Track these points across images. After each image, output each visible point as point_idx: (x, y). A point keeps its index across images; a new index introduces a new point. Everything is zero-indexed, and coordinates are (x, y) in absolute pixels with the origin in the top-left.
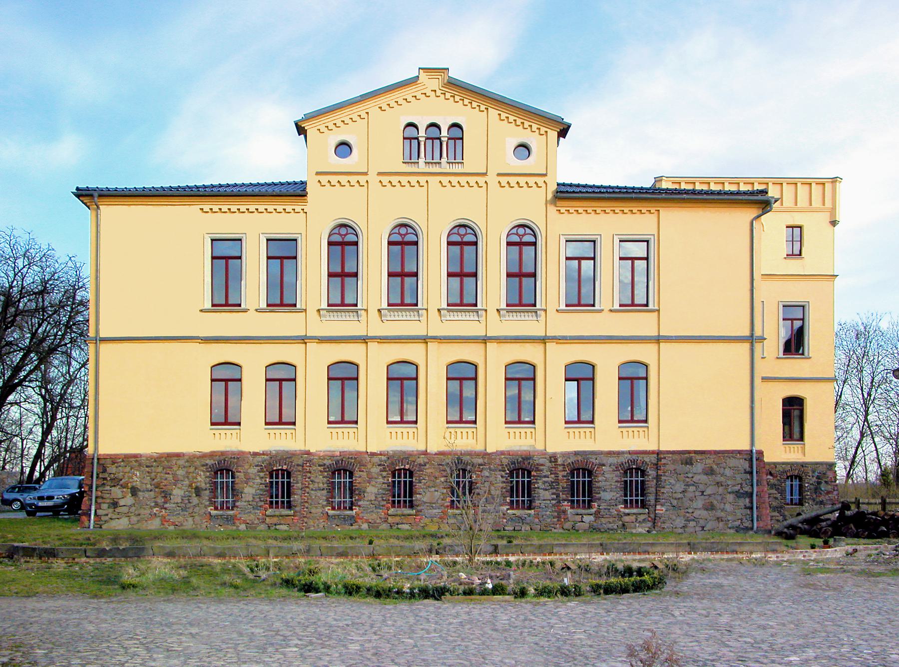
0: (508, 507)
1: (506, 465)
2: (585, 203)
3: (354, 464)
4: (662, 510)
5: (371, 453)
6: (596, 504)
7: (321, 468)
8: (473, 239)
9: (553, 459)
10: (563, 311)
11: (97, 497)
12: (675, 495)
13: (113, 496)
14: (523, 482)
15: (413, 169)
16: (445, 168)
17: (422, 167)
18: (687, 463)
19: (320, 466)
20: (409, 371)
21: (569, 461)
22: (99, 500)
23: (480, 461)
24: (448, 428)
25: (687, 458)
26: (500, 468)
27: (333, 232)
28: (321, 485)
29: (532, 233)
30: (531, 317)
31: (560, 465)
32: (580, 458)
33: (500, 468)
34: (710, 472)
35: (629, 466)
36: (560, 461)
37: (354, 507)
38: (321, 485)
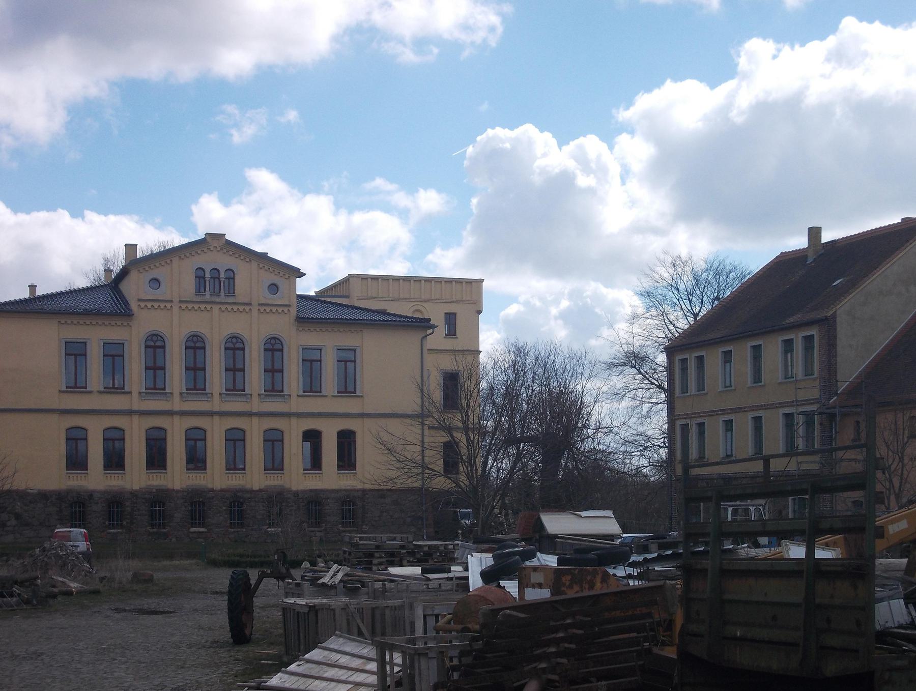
0: (267, 527)
5: (177, 490)
6: (324, 525)
7: (143, 501)
8: (241, 346)
9: (296, 495)
10: (63, 392)
15: (199, 299)
16: (222, 298)
17: (222, 298)
20: (116, 435)
21: (306, 496)
23: (248, 495)
28: (144, 512)
31: (300, 498)
33: (262, 500)
36: (301, 496)
37: (166, 527)
38: (144, 512)
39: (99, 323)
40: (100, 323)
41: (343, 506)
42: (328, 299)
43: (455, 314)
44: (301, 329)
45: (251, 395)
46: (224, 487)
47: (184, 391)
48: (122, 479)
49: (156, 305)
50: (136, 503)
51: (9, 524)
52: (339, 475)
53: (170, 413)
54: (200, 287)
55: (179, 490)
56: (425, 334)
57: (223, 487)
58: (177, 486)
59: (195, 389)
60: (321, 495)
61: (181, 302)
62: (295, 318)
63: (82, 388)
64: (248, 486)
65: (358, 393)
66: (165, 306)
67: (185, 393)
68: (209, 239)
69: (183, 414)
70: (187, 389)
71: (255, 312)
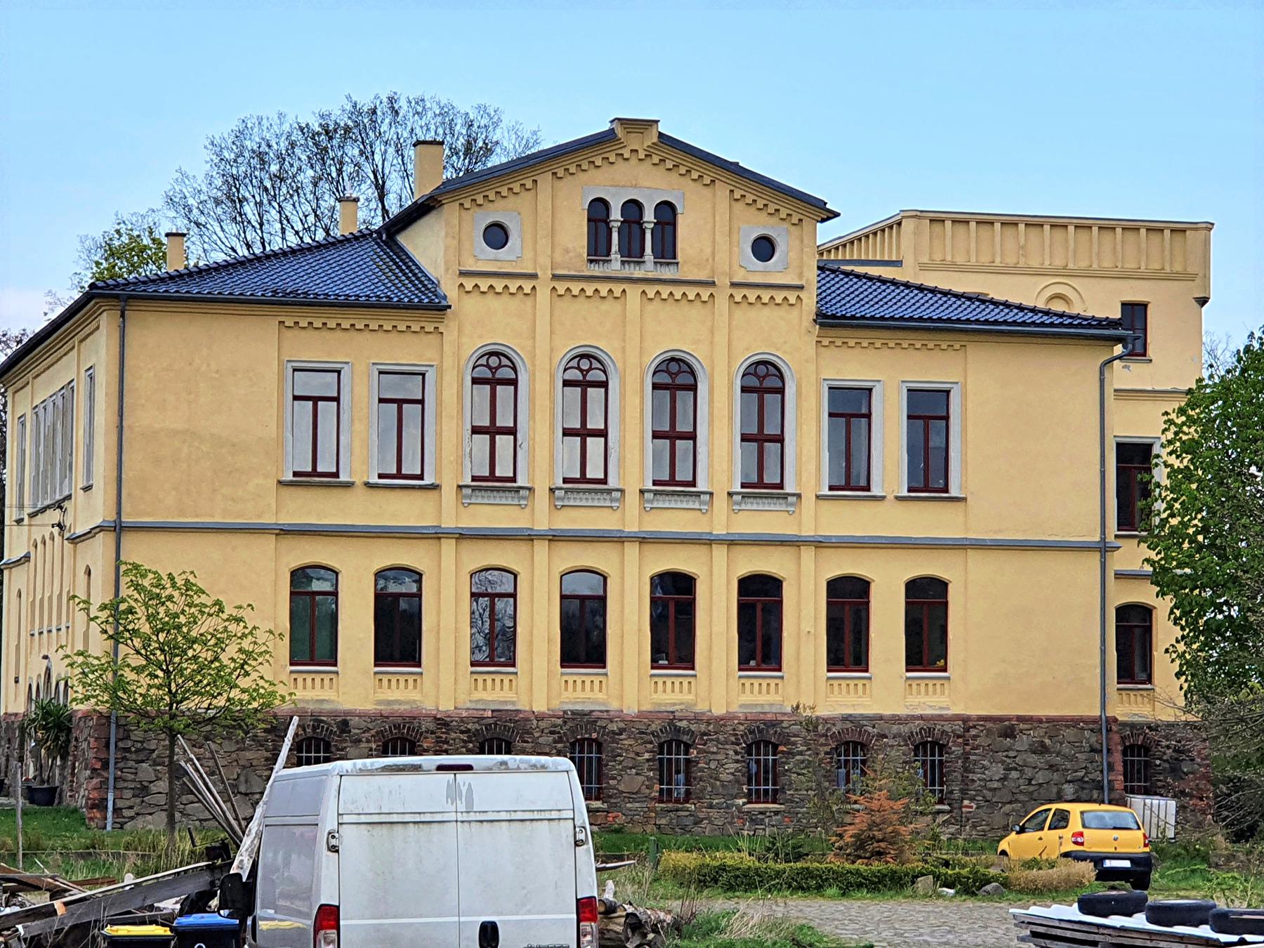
0: (745, 800)
1: (742, 736)
2: (901, 334)
3: (513, 731)
4: (971, 807)
11: (115, 779)
12: (990, 785)
13: (142, 776)
14: (766, 761)
17: (615, 265)
18: (1006, 736)
19: (462, 732)
22: (121, 784)
23: (703, 728)
24: (562, 674)
25: (1007, 728)
26: (733, 739)
27: (479, 362)
29: (510, 364)
30: (778, 506)
32: (849, 725)
34: (1041, 749)
35: (922, 737)
39: (385, 328)
40: (318, 324)
41: (661, 753)
42: (874, 271)
43: (1144, 306)
44: (826, 342)
45: (711, 494)
46: (646, 707)
47: (650, 486)
48: (415, 687)
49: (499, 285)
50: (446, 742)
51: (153, 788)
52: (910, 682)
53: (617, 539)
54: (598, 249)
55: (543, 713)
56: (1108, 357)
57: (644, 708)
58: (540, 706)
59: (673, 481)
60: (870, 729)
61: (555, 277)
62: (813, 316)
63: (863, 489)
64: (701, 707)
65: (954, 492)
66: (582, 290)
67: (561, 489)
68: (620, 132)
69: (555, 538)
70: (655, 483)
71: (722, 302)
